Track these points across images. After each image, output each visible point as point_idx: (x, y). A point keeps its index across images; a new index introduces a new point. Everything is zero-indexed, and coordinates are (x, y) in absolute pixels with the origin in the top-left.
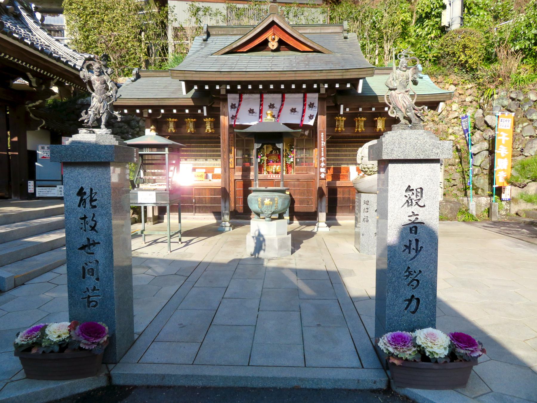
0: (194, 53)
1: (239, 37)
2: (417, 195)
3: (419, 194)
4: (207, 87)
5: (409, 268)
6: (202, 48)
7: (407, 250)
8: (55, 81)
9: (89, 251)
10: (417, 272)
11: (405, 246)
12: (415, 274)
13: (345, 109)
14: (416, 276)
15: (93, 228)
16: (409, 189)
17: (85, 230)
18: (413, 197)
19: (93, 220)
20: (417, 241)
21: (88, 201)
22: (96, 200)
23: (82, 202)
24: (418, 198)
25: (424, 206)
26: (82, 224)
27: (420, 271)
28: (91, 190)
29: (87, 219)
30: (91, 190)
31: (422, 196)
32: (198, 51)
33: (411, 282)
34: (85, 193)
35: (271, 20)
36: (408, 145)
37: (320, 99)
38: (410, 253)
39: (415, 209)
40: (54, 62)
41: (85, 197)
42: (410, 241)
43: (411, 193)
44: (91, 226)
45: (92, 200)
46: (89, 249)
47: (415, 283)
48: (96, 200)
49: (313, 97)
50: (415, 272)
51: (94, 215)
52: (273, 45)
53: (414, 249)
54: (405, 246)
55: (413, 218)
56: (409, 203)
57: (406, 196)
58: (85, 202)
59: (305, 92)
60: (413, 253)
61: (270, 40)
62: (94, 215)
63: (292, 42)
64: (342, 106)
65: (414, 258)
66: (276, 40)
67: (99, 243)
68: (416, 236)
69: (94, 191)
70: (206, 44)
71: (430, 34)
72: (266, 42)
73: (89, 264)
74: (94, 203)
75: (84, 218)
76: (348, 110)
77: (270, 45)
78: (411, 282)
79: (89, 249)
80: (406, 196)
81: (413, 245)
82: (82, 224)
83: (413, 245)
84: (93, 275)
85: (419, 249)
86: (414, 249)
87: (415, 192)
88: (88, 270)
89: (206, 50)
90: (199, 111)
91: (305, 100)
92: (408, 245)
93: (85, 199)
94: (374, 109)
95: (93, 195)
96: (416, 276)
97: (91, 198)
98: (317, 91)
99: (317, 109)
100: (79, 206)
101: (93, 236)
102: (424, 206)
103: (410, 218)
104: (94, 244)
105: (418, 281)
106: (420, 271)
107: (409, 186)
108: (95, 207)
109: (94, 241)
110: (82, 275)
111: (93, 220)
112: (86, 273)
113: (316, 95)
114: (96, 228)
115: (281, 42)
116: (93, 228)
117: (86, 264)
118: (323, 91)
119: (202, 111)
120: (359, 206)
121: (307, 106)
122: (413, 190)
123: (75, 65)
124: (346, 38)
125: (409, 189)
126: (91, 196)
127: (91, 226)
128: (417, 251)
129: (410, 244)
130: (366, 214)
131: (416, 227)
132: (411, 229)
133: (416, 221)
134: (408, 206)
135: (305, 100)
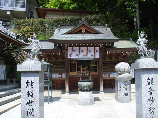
0: (56, 34)
1: (72, 29)
2: (151, 81)
3: (152, 81)
4: (61, 45)
5: (150, 107)
6: (59, 32)
7: (149, 101)
8: (7, 43)
9: (30, 105)
10: (153, 109)
11: (149, 99)
12: (153, 110)
13: (108, 52)
14: (153, 110)
15: (32, 96)
16: (148, 79)
17: (29, 97)
18: (150, 82)
19: (32, 93)
20: (152, 97)
21: (30, 85)
22: (33, 85)
23: (28, 86)
24: (152, 82)
25: (154, 85)
26: (27, 94)
27: (154, 109)
28: (32, 81)
29: (29, 93)
30: (32, 81)
31: (153, 81)
32: (57, 33)
33: (151, 112)
34: (29, 83)
35: (83, 23)
36: (148, 64)
37: (100, 49)
38: (150, 102)
39: (151, 86)
40: (8, 36)
41: (29, 84)
42: (150, 98)
43: (149, 80)
44: (31, 95)
45: (31, 85)
46: (30, 104)
47: (153, 113)
48: (33, 85)
49: (98, 48)
50: (152, 109)
51: (32, 91)
52: (83, 31)
53: (151, 100)
54: (149, 99)
55: (151, 89)
56: (149, 84)
57: (148, 82)
58: (29, 86)
59: (95, 47)
60: (151, 102)
61: (82, 30)
62: (32, 91)
63: (90, 31)
64: (107, 52)
65: (152, 104)
66: (84, 30)
67: (34, 102)
68: (152, 96)
69: (32, 82)
70: (60, 31)
71: (28, 31)
72: (81, 30)
73: (30, 110)
74: (32, 86)
75: (28, 92)
76: (109, 52)
77: (82, 31)
78: (151, 112)
79: (30, 104)
80: (148, 82)
81: (151, 99)
82: (27, 94)
83: (151, 99)
84: (31, 114)
85: (153, 100)
86: (151, 100)
87: (150, 80)
88: (29, 112)
89: (60, 33)
90: (58, 53)
91: (95, 49)
92: (149, 99)
93: (29, 85)
94: (118, 52)
95: (32, 83)
96: (153, 110)
97: (31, 84)
98: (99, 46)
99: (99, 52)
100: (27, 87)
101: (32, 99)
102: (154, 85)
103: (149, 89)
104: (32, 102)
105: (154, 112)
106: (154, 109)
107: (149, 78)
108: (33, 88)
109: (32, 101)
110: (27, 114)
111: (32, 93)
112: (29, 114)
113: (99, 48)
114: (33, 96)
115: (86, 30)
116: (32, 96)
117: (29, 110)
118: (101, 46)
119: (59, 53)
120: (117, 86)
121: (88, 51)
122: (150, 79)
123: (14, 37)
124: (107, 29)
125: (148, 79)
126: (31, 83)
127: (31, 95)
128: (153, 101)
129: (150, 99)
130: (120, 88)
131: (152, 92)
132: (150, 93)
133: (152, 90)
134: (149, 85)
135: (95, 49)
